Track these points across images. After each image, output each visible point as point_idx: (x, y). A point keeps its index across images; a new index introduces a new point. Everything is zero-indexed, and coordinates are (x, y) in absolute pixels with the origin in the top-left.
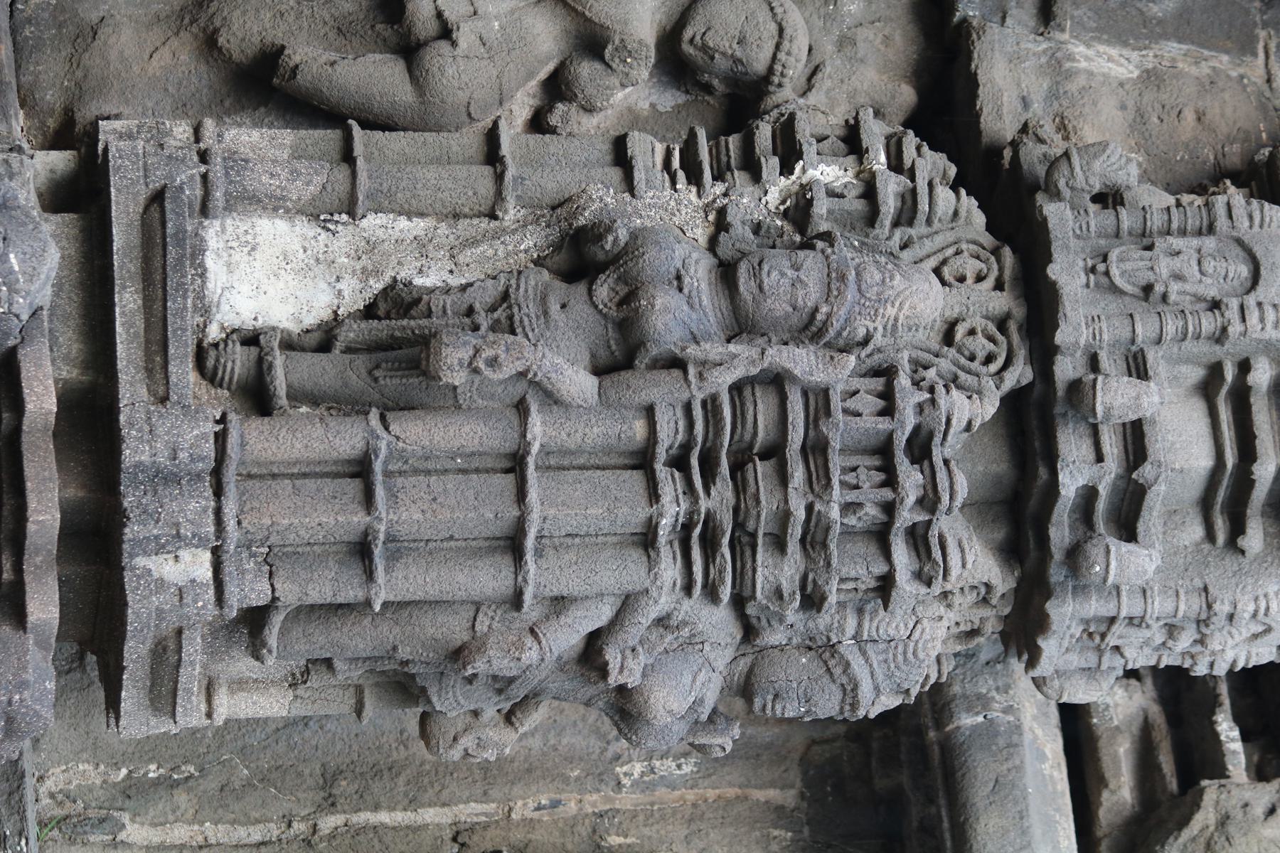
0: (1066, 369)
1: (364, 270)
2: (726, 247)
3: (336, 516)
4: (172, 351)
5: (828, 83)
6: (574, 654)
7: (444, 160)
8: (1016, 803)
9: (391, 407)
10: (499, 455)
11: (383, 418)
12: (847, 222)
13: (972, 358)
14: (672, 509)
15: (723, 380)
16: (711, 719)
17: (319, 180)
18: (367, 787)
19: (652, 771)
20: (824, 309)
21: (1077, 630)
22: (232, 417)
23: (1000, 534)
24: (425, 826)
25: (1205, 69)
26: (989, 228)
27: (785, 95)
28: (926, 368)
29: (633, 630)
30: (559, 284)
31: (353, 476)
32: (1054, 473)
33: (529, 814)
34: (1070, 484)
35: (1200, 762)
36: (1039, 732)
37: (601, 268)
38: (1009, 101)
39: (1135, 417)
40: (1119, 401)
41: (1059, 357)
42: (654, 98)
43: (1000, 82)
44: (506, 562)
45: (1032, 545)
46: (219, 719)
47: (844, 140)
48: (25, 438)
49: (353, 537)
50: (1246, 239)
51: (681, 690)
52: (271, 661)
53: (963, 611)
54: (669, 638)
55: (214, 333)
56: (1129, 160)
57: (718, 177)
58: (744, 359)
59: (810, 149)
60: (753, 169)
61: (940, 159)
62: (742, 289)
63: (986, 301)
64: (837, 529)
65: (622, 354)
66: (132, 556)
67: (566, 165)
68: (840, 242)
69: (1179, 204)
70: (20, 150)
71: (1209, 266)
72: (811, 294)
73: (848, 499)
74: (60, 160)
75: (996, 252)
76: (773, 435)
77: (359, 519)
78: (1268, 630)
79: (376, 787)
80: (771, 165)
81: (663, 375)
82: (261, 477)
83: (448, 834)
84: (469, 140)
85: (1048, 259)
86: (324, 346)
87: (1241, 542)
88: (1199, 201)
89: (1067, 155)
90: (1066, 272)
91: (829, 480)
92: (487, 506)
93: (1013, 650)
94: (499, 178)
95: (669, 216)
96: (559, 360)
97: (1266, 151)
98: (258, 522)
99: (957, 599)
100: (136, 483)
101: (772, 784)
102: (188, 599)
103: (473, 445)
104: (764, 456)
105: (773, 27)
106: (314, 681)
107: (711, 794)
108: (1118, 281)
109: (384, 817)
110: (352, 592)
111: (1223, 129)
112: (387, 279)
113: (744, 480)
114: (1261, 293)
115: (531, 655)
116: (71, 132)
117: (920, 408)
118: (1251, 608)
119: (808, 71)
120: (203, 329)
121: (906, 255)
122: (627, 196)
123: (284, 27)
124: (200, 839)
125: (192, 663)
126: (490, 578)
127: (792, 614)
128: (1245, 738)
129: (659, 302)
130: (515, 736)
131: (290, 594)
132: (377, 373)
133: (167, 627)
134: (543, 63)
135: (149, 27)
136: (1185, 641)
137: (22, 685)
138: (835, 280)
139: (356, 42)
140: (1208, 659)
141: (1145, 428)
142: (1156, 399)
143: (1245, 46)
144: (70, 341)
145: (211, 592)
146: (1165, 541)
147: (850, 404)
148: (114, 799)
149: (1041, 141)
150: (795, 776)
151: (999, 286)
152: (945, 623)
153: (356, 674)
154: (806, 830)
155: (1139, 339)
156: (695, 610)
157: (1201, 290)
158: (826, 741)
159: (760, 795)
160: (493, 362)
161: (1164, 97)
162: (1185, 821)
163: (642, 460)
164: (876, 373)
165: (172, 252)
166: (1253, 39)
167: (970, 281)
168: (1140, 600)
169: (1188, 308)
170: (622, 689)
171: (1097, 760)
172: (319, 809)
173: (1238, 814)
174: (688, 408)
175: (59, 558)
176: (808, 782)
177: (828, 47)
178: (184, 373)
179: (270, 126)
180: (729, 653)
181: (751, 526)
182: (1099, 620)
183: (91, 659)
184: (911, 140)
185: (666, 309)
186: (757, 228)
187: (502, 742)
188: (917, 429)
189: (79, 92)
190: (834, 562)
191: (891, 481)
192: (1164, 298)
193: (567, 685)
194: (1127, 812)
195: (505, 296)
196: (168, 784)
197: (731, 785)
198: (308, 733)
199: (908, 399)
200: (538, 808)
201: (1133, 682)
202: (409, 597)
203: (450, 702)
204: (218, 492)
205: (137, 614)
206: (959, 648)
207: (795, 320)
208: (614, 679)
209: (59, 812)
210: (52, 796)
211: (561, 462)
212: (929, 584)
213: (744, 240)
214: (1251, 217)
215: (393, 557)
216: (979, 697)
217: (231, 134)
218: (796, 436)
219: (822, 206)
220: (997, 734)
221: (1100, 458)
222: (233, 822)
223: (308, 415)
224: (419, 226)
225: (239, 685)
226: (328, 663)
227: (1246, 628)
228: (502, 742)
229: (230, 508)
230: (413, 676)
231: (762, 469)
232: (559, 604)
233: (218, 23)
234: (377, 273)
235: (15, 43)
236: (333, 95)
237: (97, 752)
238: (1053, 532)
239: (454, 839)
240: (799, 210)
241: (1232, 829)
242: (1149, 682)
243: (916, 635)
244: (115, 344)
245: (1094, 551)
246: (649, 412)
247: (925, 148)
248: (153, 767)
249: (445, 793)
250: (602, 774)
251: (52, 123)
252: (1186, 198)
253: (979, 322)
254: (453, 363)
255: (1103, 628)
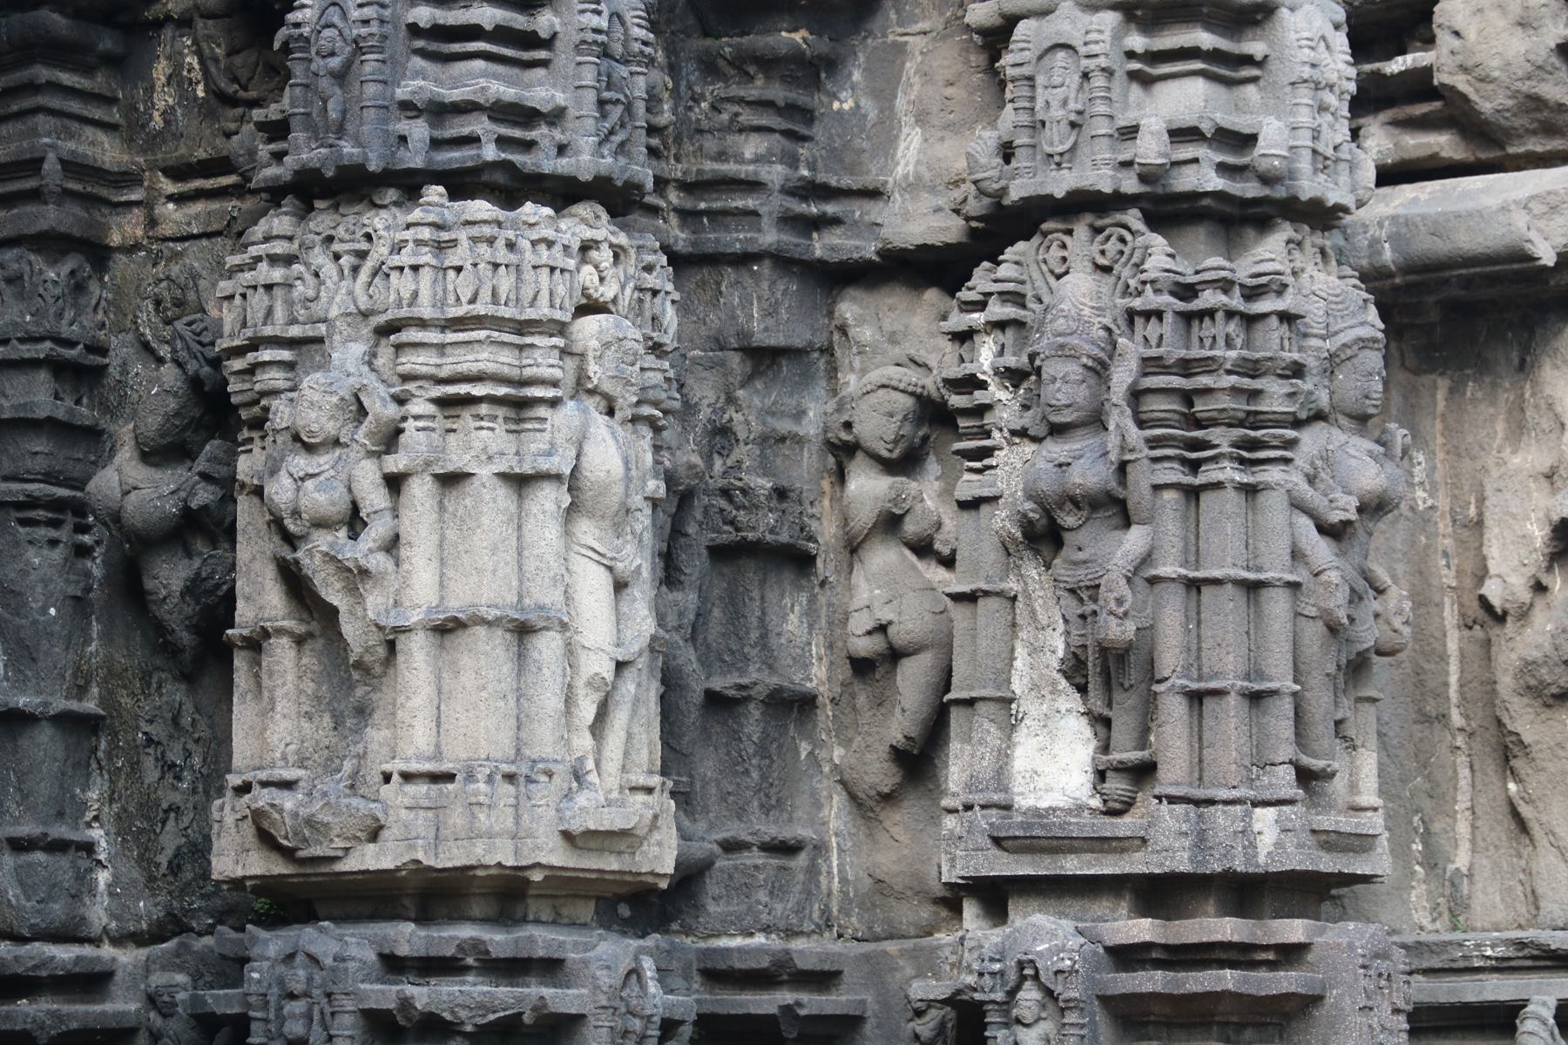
0: (1130, 185)
1: (1051, 693)
2: (1039, 430)
3: (1230, 717)
4: (1108, 834)
5: (922, 352)
6: (1333, 544)
7: (973, 633)
8: (1448, 220)
9: (1152, 677)
10: (1188, 597)
11: (1159, 682)
12: (1022, 342)
13: (1122, 253)
14: (1228, 472)
15: (1135, 435)
16: (1383, 445)
17: (986, 725)
18: (1432, 691)
19: (1422, 483)
20: (1085, 360)
21: (1322, 177)
22: (1157, 791)
23: (1250, 233)
24: (1461, 650)
25: (916, 80)
26: (1027, 239)
27: (930, 384)
28: (1128, 286)
29: (1317, 501)
30: (1064, 552)
31: (1201, 704)
32: (1206, 194)
33: (1452, 573)
34: (1214, 182)
35: (1420, 85)
36: (1397, 202)
37: (1052, 521)
38: (937, 222)
39: (1166, 136)
40: (1154, 146)
41: (1122, 190)
42: (932, 478)
43: (923, 228)
44: (1266, 593)
45: (1259, 210)
46: (1378, 802)
47: (962, 342)
48: (1171, 941)
49: (1246, 704)
50: (1038, 53)
51: (1361, 466)
52: (1336, 765)
53: (1306, 260)
54: (1323, 475)
55: (1096, 803)
56: (980, 137)
57: (988, 435)
58: (1120, 419)
59: (969, 368)
60: (982, 410)
61: (978, 272)
62: (1069, 420)
63: (1080, 242)
64: (1245, 353)
65: (1114, 507)
66: (1258, 866)
67: (980, 543)
68: (1036, 348)
69: (1012, 101)
70: (962, 939)
71: (1057, 80)
72: (1073, 370)
73: (1222, 344)
74: (970, 910)
75: (1045, 234)
76: (1175, 398)
77: (1233, 700)
78: (1323, 38)
79: (1431, 684)
80: (980, 397)
81: (1131, 478)
82: (1201, 770)
83: (1466, 633)
84: (959, 613)
85: (1051, 197)
86: (1107, 722)
87: (1258, 58)
88: (1010, 86)
89: (975, 182)
90: (1059, 184)
91: (1208, 358)
92: (1224, 608)
93: (1336, 223)
94: (986, 593)
95: (1016, 471)
96: (1119, 554)
97: (975, 36)
98: (1234, 773)
99: (1298, 264)
100: (1204, 862)
101: (1433, 396)
102: (1290, 825)
103: (1180, 617)
104: (1191, 404)
105: (881, 392)
106: (1351, 733)
107: (1440, 440)
108: (1067, 146)
109: (1453, 679)
110: (1287, 706)
111: (960, 67)
112: (1059, 676)
113: (1208, 419)
114: (1077, 42)
115: (1333, 576)
116: (951, 900)
117: (1157, 291)
118: (1307, 51)
119: (913, 366)
120: (1093, 810)
121: (1046, 300)
122: (1001, 501)
123: (877, 745)
124: (1468, 813)
125: (1337, 822)
126: (1277, 605)
127: (1305, 385)
128: (1403, 52)
129: (1078, 481)
130: (1394, 589)
131: (1286, 751)
132: (1127, 685)
133: (1310, 841)
134: (905, 558)
135: (876, 842)
136: (1331, 99)
137: (1351, 946)
138: (1064, 352)
139: (888, 693)
140: (1344, 82)
141: (1175, 127)
142: (1153, 120)
143: (900, 50)
144: (1101, 907)
145: (1284, 808)
146: (1258, 113)
147: (1153, 342)
148: (1437, 875)
149: (965, 200)
150: (1427, 379)
151: (1070, 232)
152: (1315, 273)
153: (1346, 702)
154: (1469, 372)
155: (1110, 131)
156: (1301, 457)
157: (1075, 86)
158: (1402, 355)
159: (1441, 404)
160: (1119, 601)
161: (935, 109)
162: (1464, 98)
163: (1192, 493)
164: (1131, 323)
165: (1037, 832)
166: (895, 44)
167: (1065, 254)
168: (1300, 132)
169: (1087, 95)
170: (1360, 510)
171: (1418, 160)
172: (1446, 726)
173: (1459, 59)
174: (1155, 460)
175: (1259, 918)
176: (1432, 371)
177: (897, 352)
178: (1125, 825)
179: (947, 755)
180: (1335, 431)
181: (1241, 415)
182: (1314, 162)
183: (1334, 892)
184: (964, 295)
185: (1083, 475)
186: (1026, 407)
187: (1398, 599)
188: (1172, 293)
189: (922, 893)
190: (1269, 354)
191: (1210, 313)
192: (1080, 113)
193: (1357, 549)
194: (1457, 138)
195: (1072, 591)
196: (1427, 838)
197: (1433, 426)
198: (1391, 734)
199: (1150, 300)
200: (1448, 566)
201: (1362, 132)
202: (1291, 665)
203: (1368, 635)
204: (1211, 802)
205: (1300, 862)
206: (1334, 263)
207: (1092, 381)
208: (1352, 516)
209: (1446, 915)
210: (1434, 920)
211: (1193, 552)
212: (1286, 286)
213: (1034, 418)
214: (1022, 50)
215: (1261, 675)
216: (1370, 246)
217: (952, 787)
218: (1176, 382)
219: (1011, 361)
220: (1398, 234)
221: (1196, 161)
222: (1456, 789)
223: (1157, 736)
224: (1021, 652)
225: (1353, 787)
226: (1338, 723)
227: (1322, 55)
228: (1398, 599)
229: (1224, 794)
230: (1349, 662)
231: (1200, 406)
232: (1297, 555)
233: (873, 793)
234: (1054, 683)
235: (886, 939)
236: (925, 712)
237: (1403, 887)
238: (1250, 195)
239: (1470, 628)
240: (1014, 377)
241: (1470, 63)
242: (1362, 121)
243: (1324, 295)
244: (1103, 875)
245: (1263, 165)
246: (1157, 488)
247: (969, 284)
248: (1414, 847)
249: (1437, 634)
250: (1424, 520)
251: (944, 913)
252: (1008, 96)
253: (1096, 247)
254: (1118, 631)
255: (1320, 158)
